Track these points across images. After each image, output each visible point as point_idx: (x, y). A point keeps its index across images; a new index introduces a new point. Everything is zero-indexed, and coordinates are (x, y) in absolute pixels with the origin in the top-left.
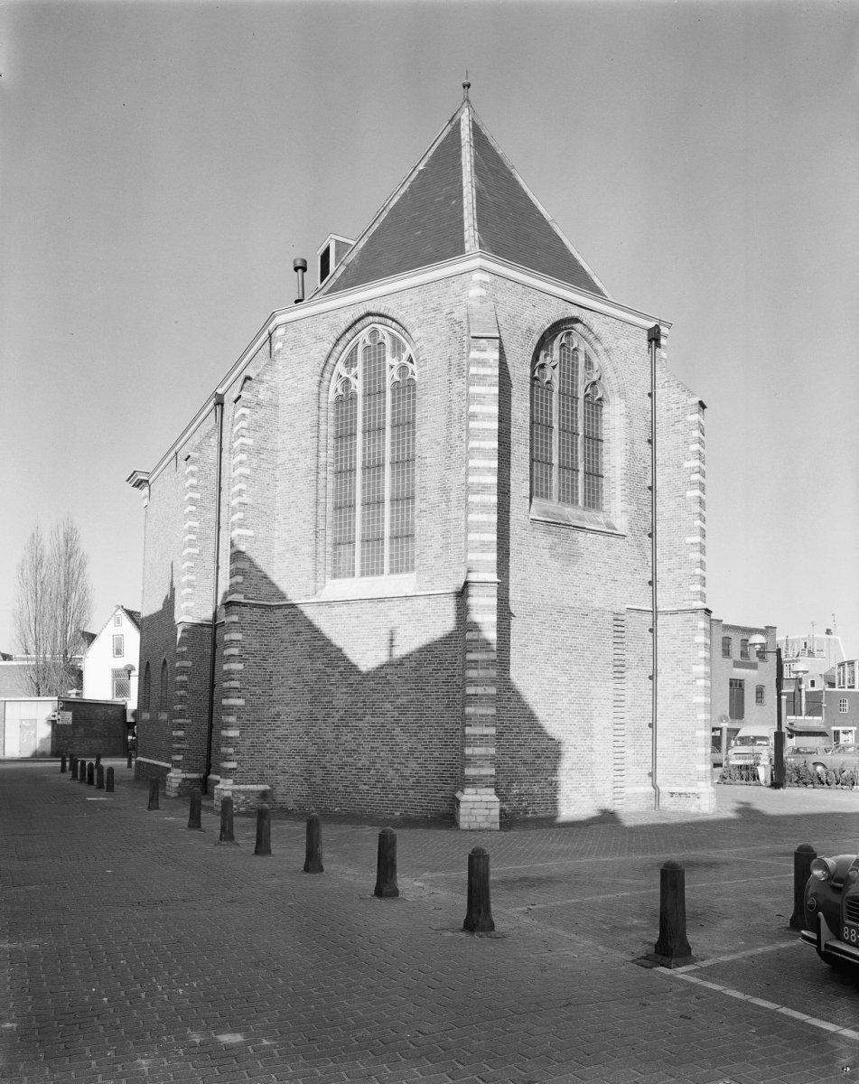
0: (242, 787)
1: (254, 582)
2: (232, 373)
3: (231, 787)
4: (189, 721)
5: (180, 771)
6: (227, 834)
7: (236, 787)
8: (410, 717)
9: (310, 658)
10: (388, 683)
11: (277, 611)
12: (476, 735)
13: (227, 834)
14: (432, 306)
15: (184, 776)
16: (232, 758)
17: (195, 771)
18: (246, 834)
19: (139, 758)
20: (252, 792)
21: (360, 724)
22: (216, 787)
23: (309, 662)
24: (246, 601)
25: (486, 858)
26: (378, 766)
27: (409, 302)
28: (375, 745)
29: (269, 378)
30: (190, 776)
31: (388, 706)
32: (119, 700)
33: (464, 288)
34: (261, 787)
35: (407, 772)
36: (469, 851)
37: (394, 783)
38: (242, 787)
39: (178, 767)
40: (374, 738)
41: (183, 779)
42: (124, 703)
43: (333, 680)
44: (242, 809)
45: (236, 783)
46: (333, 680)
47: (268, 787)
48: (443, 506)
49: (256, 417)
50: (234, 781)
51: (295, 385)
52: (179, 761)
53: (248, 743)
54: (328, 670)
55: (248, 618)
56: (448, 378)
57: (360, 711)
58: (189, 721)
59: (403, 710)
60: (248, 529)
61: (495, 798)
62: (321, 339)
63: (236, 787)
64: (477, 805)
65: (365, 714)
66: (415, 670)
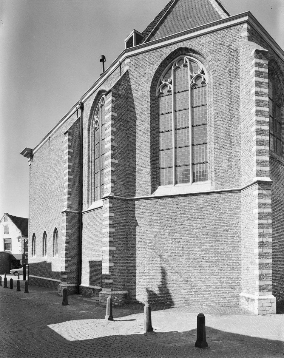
0: (116, 292)
1: (119, 187)
2: (69, 114)
3: (111, 293)
4: (70, 259)
5: (66, 283)
6: (19, 290)
7: (113, 293)
8: (210, 254)
9: (150, 226)
10: (197, 237)
11: (130, 202)
12: (263, 264)
13: (19, 290)
14: (219, 42)
15: (68, 285)
16: (110, 277)
17: (71, 283)
18: (23, 290)
19: (30, 276)
20: (121, 294)
21: (181, 259)
22: (100, 292)
23: (149, 227)
24: (115, 196)
25: (204, 317)
26: (192, 280)
27: (205, 41)
28: (191, 269)
29: (123, 83)
30: (71, 285)
31: (197, 249)
32: (7, 251)
33: (238, 32)
34: (124, 292)
35: (210, 283)
36: (198, 314)
37: (203, 289)
38: (116, 292)
39: (64, 281)
40: (190, 267)
41: (68, 287)
42: (9, 252)
43: (164, 236)
44: (116, 304)
45: (112, 290)
46: (164, 236)
47: (127, 292)
48: (228, 145)
49: (118, 102)
50: (112, 289)
51: (137, 88)
52: (66, 278)
53: (117, 269)
54: (162, 232)
55: (116, 205)
56: (229, 79)
57: (181, 252)
58: (70, 259)
59: (206, 251)
60: (115, 159)
61: (273, 297)
62: (153, 63)
63: (113, 293)
64: (266, 301)
65: (183, 254)
66: (214, 230)
